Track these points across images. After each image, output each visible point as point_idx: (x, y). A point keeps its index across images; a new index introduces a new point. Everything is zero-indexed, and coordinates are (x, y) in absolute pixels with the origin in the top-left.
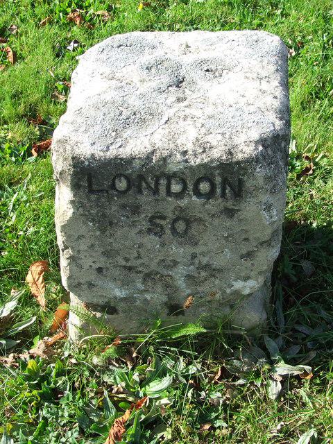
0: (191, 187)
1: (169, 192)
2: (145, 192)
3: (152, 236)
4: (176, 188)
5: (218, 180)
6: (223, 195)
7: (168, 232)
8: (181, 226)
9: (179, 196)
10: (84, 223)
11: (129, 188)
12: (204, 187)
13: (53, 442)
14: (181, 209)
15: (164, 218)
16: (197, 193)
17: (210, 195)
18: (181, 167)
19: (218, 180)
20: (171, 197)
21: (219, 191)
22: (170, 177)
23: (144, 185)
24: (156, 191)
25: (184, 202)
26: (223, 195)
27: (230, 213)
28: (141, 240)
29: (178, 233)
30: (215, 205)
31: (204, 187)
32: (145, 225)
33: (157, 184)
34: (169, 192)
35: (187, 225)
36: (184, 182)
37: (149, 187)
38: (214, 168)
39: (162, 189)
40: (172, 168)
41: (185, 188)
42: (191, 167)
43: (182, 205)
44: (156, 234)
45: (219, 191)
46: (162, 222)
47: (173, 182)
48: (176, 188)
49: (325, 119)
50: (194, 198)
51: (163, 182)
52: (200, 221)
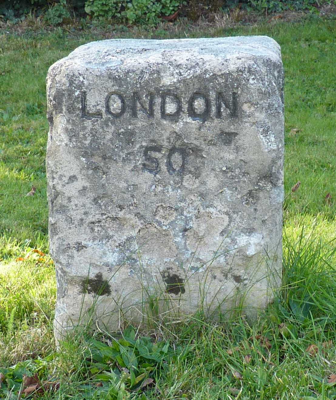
0: (185, 107)
1: (164, 115)
2: (140, 114)
3: (147, 174)
4: (171, 108)
5: (213, 95)
6: (219, 114)
7: (164, 168)
8: (177, 158)
9: (175, 117)
10: (77, 158)
11: (123, 110)
12: (199, 104)
13: (168, 2)
14: (178, 136)
15: (158, 149)
16: (192, 113)
17: (205, 116)
18: (175, 80)
19: (213, 95)
20: (165, 119)
21: (214, 109)
22: (166, 93)
23: (139, 105)
24: (151, 114)
25: (178, 127)
26: (219, 114)
27: (228, 138)
28: (135, 180)
29: (174, 170)
30: (214, 126)
31: (199, 104)
32: (140, 160)
33: (152, 104)
34: (164, 115)
35: (183, 159)
36: (177, 99)
37: (143, 108)
38: (208, 80)
39: (157, 109)
40: (167, 80)
41: (179, 109)
42: (184, 80)
43: (177, 129)
44: (151, 171)
45: (214, 109)
46: (158, 155)
47: (168, 100)
48: (171, 108)
49: (331, 108)
50: (189, 120)
51: (158, 101)
52: (197, 151)
